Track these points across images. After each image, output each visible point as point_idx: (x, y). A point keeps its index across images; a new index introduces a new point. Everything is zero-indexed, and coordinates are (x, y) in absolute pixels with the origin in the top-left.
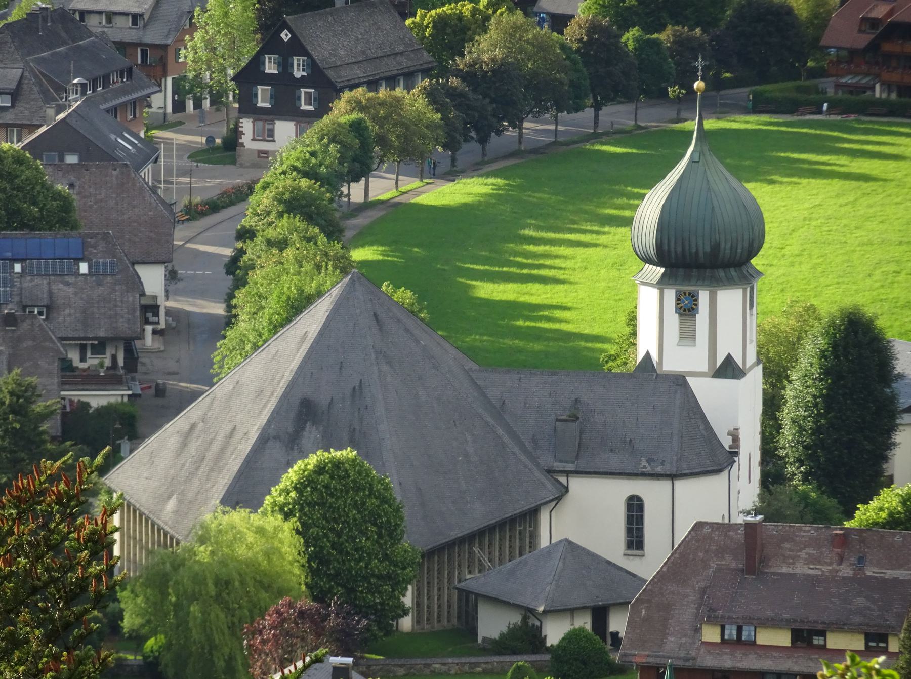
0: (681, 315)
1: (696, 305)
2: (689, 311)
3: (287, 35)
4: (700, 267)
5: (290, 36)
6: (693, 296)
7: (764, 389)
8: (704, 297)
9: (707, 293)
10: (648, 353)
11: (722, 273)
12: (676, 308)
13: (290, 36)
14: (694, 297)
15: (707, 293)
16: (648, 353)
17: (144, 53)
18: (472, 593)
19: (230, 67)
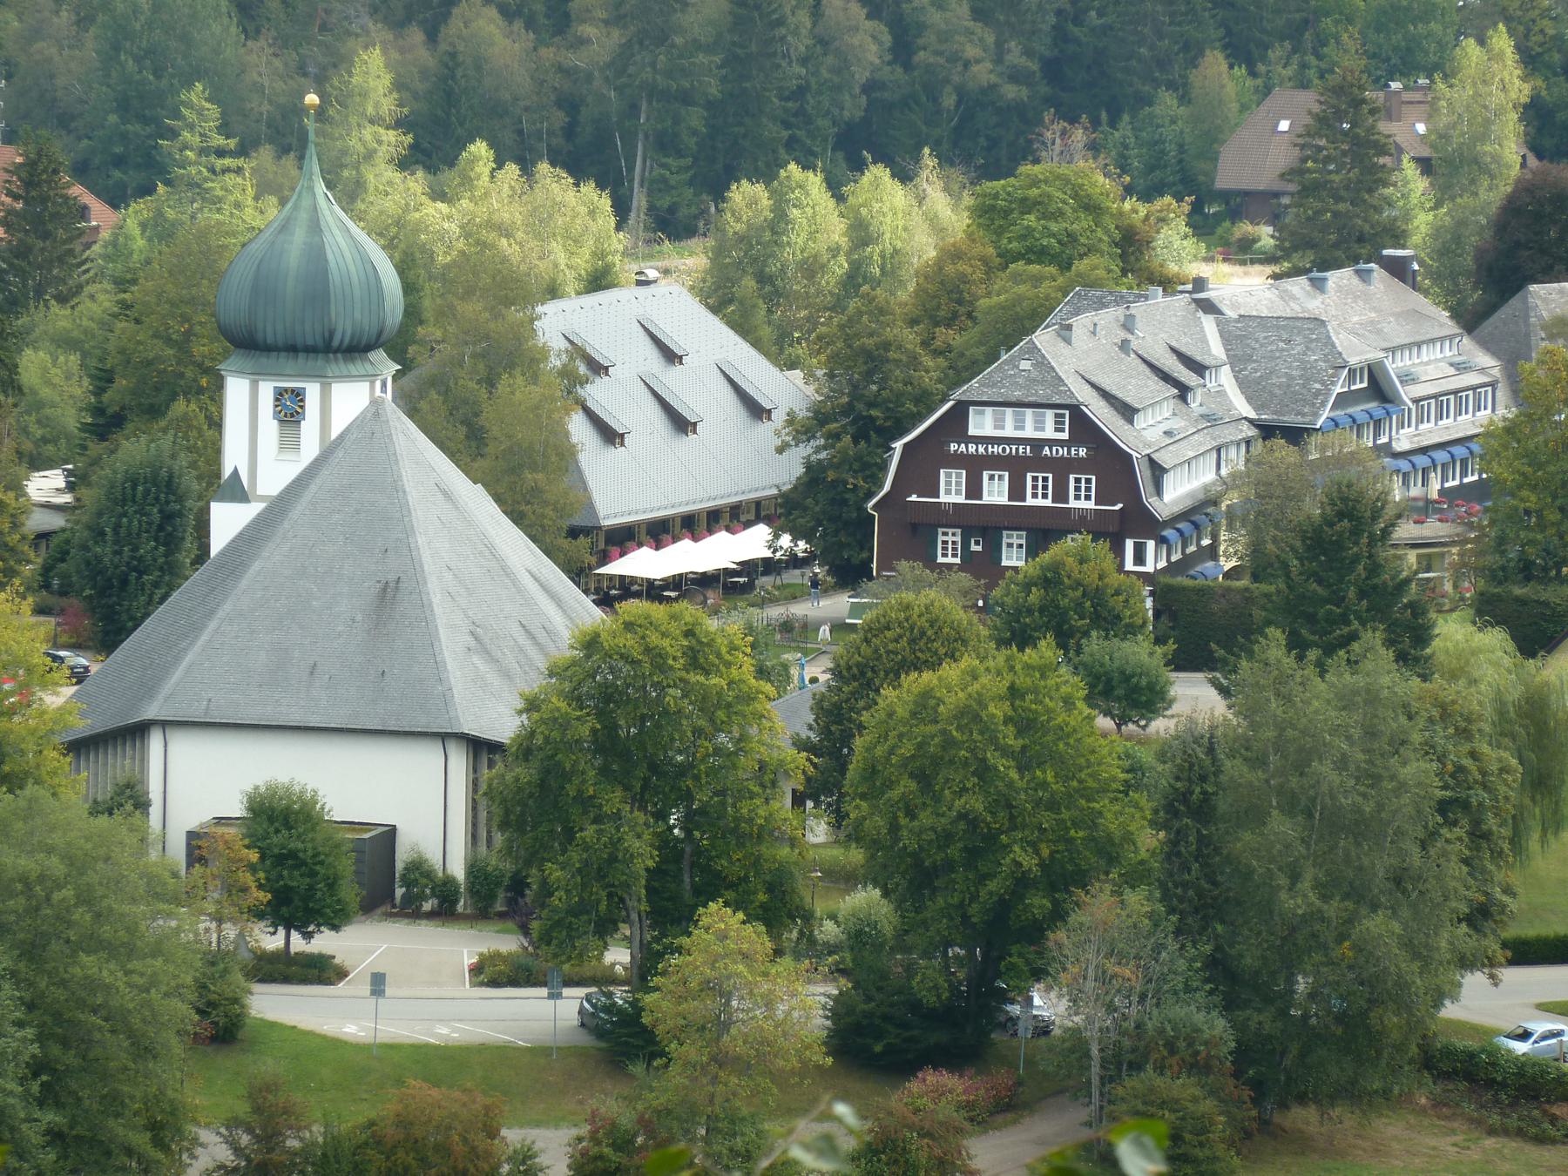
0: (281, 421)
1: (302, 407)
2: (292, 415)
3: (977, 543)
4: (311, 350)
5: (959, 531)
6: (298, 395)
7: (594, 601)
8: (312, 391)
9: (317, 386)
10: (236, 469)
11: (331, 355)
12: (275, 412)
13: (959, 531)
14: (298, 395)
15: (317, 386)
16: (236, 469)
17: (1239, 372)
18: (431, 915)
19: (1186, 69)
